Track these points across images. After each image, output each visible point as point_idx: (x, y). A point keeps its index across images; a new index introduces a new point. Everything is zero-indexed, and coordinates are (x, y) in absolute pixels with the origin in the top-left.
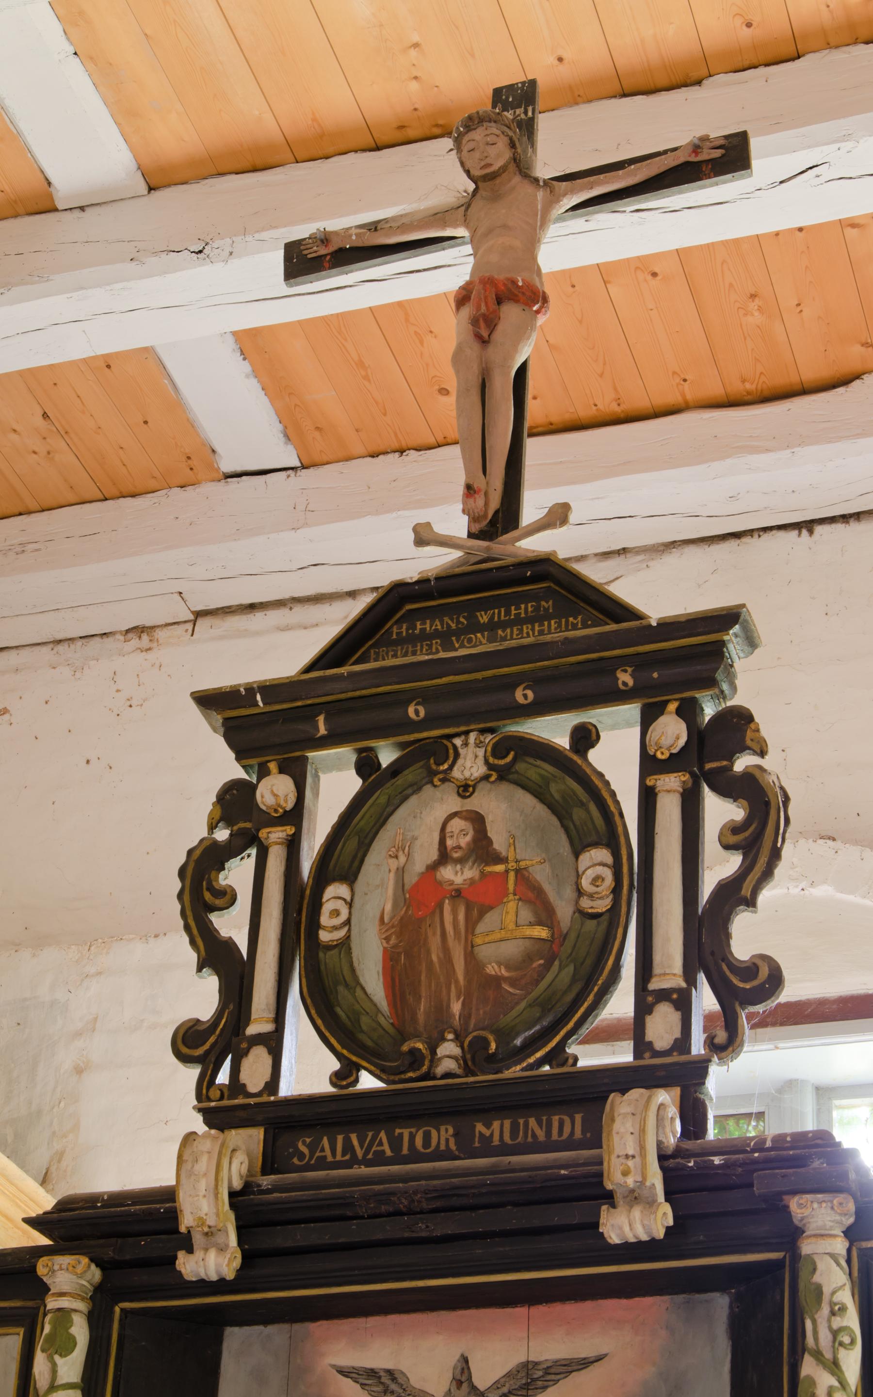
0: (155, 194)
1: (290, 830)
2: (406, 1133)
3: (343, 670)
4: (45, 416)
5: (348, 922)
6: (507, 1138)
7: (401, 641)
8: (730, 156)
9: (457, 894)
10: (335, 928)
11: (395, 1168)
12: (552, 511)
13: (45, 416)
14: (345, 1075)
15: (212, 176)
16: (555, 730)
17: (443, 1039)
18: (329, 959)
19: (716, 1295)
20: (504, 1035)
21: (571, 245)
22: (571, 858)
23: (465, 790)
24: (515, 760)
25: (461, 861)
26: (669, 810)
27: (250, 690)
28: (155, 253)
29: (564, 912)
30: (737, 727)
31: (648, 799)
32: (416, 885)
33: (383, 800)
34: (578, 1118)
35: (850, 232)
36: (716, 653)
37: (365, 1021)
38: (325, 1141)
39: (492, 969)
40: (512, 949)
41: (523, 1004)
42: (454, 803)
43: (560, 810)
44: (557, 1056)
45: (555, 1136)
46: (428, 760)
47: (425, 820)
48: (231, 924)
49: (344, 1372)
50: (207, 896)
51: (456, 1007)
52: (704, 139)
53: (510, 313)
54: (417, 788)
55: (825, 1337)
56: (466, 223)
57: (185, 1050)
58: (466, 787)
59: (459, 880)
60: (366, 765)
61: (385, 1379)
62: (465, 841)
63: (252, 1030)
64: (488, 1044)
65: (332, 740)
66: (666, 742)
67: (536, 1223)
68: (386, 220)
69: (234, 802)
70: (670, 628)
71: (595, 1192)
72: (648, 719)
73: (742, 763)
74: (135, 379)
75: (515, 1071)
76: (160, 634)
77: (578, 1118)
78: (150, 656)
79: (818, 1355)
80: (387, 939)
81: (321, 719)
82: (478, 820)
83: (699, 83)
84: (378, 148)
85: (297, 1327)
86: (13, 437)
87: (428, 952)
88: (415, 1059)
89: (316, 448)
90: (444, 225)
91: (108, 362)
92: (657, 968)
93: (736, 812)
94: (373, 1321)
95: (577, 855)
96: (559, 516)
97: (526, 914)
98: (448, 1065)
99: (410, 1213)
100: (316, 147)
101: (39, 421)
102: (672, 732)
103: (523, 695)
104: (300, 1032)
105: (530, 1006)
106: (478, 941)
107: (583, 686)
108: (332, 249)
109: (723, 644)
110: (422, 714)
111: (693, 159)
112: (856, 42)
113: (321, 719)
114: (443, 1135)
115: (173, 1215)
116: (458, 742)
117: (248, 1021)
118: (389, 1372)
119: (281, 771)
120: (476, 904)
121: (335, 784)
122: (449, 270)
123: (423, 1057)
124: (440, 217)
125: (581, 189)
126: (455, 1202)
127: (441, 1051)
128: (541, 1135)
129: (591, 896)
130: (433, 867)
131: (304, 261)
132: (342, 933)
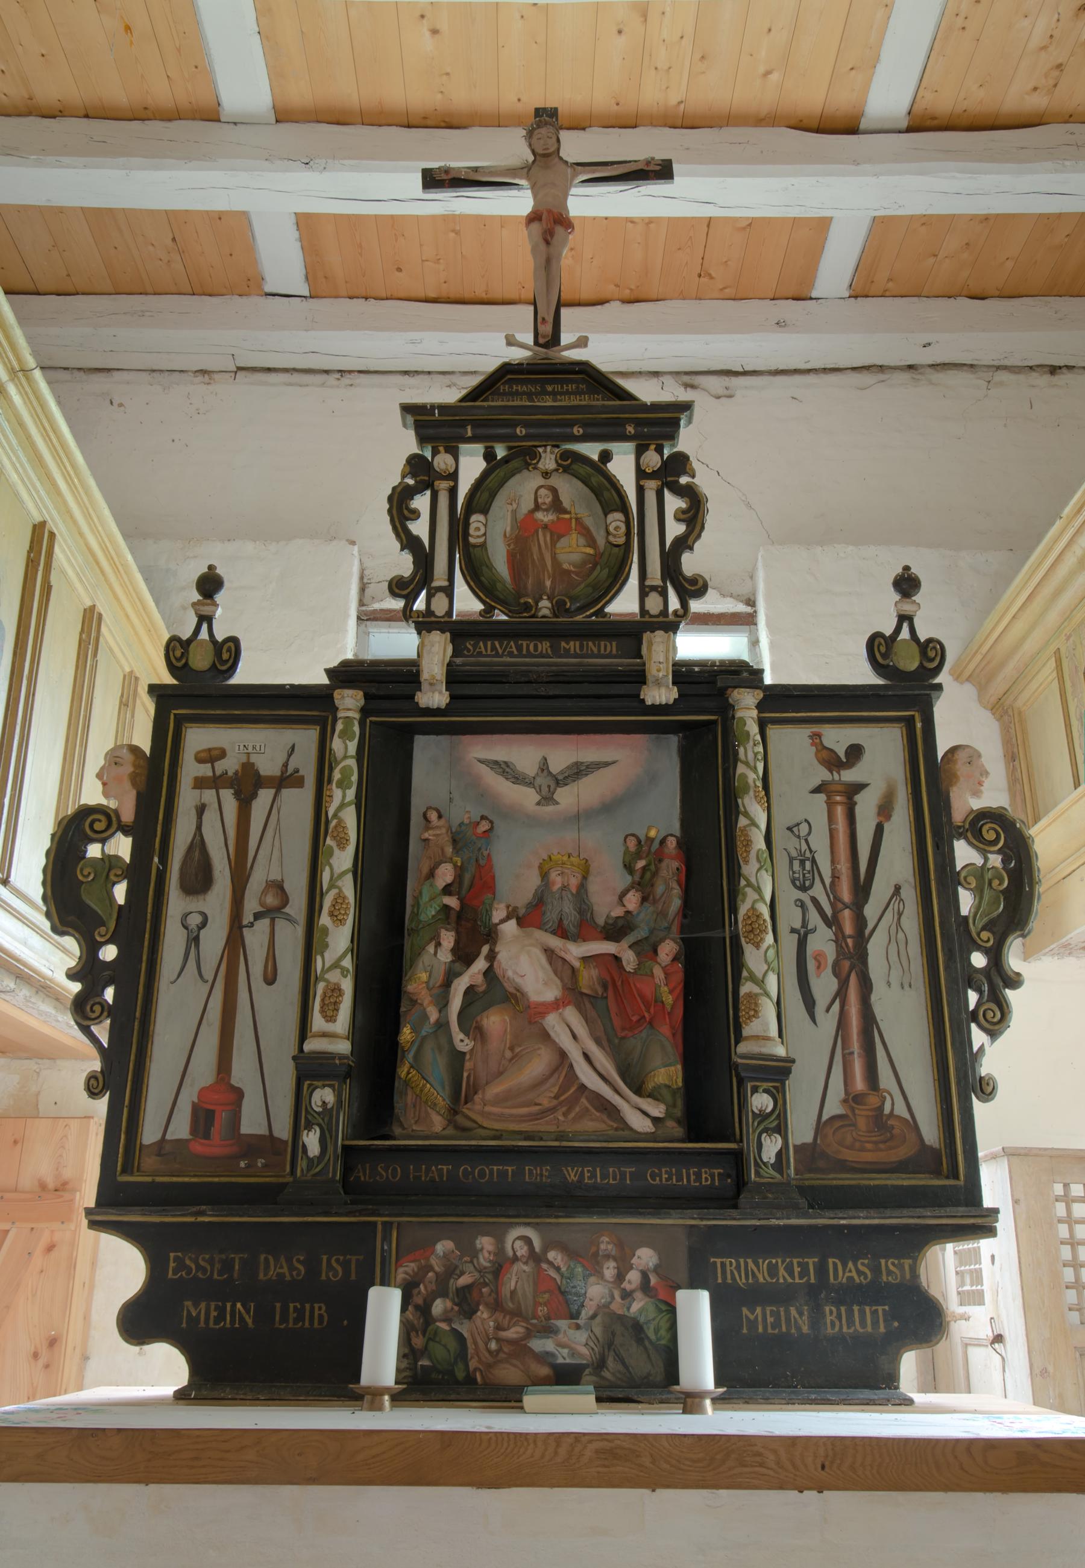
0: (280, 125)
1: (452, 484)
2: (524, 644)
3: (477, 403)
4: (174, 239)
5: (485, 534)
6: (578, 651)
7: (505, 394)
8: (663, 171)
9: (545, 527)
10: (478, 537)
11: (527, 660)
12: (579, 339)
13: (174, 239)
14: (489, 610)
15: (313, 122)
16: (591, 450)
17: (542, 599)
18: (477, 552)
19: (671, 736)
20: (573, 599)
21: (586, 203)
22: (602, 516)
23: (546, 475)
24: (571, 463)
25: (546, 510)
26: (651, 498)
27: (433, 407)
28: (281, 159)
29: (601, 542)
30: (679, 463)
31: (640, 491)
32: (523, 520)
33: (502, 474)
34: (614, 644)
35: (630, 225)
36: (675, 424)
37: (499, 586)
38: (481, 644)
39: (566, 566)
40: (576, 557)
41: (582, 586)
42: (541, 481)
43: (597, 492)
44: (600, 612)
45: (602, 652)
46: (524, 457)
47: (525, 489)
48: (420, 528)
49: (480, 761)
50: (406, 512)
51: (548, 583)
52: (653, 159)
53: (559, 230)
54: (518, 471)
55: (750, 755)
56: (528, 177)
57: (397, 591)
58: (547, 473)
59: (546, 519)
60: (489, 456)
61: (503, 766)
62: (548, 500)
63: (435, 584)
64: (566, 604)
65: (474, 439)
66: (652, 464)
67: (602, 692)
68: (482, 167)
69: (416, 465)
70: (656, 407)
71: (640, 677)
72: (640, 451)
73: (684, 480)
74: (233, 229)
75: (579, 618)
76: (216, 376)
77: (614, 644)
78: (209, 387)
79: (747, 764)
80: (509, 545)
81: (469, 428)
82: (554, 491)
83: (584, 129)
84: (409, 127)
85: (454, 737)
86: (151, 248)
87: (532, 555)
88: (527, 607)
89: (321, 284)
90: (515, 176)
91: (220, 216)
92: (649, 575)
93: (682, 504)
94: (496, 737)
95: (606, 515)
96: (582, 342)
97: (582, 541)
98: (545, 612)
99: (536, 682)
100: (449, 122)
101: (169, 242)
102: (653, 461)
103: (577, 431)
104: (461, 588)
105: (587, 586)
106: (558, 551)
107: (609, 430)
108: (450, 177)
109: (679, 419)
110: (524, 432)
111: (646, 168)
112: (665, 126)
113: (469, 428)
114: (544, 646)
115: (418, 674)
116: (541, 450)
117: (432, 580)
118: (505, 763)
119: (446, 452)
120: (556, 533)
121: (471, 465)
122: (519, 202)
123: (532, 606)
124: (513, 171)
125: (589, 172)
126: (561, 679)
127: (541, 604)
128: (595, 650)
129: (615, 536)
130: (532, 512)
131: (433, 180)
132: (482, 540)
